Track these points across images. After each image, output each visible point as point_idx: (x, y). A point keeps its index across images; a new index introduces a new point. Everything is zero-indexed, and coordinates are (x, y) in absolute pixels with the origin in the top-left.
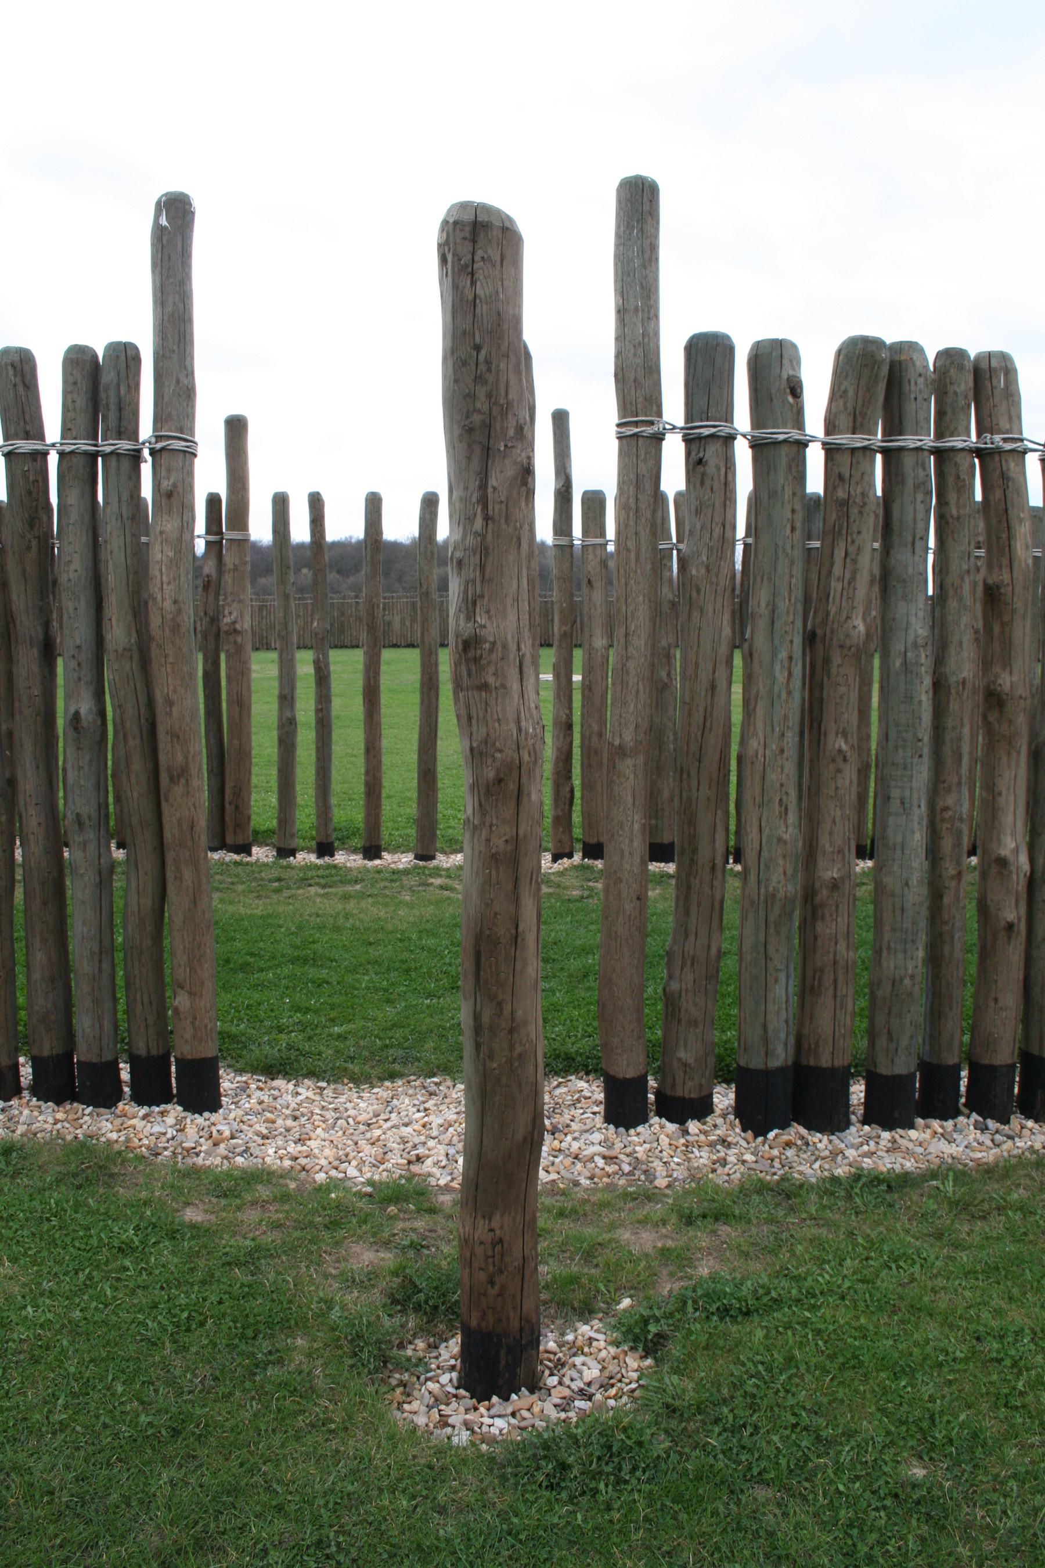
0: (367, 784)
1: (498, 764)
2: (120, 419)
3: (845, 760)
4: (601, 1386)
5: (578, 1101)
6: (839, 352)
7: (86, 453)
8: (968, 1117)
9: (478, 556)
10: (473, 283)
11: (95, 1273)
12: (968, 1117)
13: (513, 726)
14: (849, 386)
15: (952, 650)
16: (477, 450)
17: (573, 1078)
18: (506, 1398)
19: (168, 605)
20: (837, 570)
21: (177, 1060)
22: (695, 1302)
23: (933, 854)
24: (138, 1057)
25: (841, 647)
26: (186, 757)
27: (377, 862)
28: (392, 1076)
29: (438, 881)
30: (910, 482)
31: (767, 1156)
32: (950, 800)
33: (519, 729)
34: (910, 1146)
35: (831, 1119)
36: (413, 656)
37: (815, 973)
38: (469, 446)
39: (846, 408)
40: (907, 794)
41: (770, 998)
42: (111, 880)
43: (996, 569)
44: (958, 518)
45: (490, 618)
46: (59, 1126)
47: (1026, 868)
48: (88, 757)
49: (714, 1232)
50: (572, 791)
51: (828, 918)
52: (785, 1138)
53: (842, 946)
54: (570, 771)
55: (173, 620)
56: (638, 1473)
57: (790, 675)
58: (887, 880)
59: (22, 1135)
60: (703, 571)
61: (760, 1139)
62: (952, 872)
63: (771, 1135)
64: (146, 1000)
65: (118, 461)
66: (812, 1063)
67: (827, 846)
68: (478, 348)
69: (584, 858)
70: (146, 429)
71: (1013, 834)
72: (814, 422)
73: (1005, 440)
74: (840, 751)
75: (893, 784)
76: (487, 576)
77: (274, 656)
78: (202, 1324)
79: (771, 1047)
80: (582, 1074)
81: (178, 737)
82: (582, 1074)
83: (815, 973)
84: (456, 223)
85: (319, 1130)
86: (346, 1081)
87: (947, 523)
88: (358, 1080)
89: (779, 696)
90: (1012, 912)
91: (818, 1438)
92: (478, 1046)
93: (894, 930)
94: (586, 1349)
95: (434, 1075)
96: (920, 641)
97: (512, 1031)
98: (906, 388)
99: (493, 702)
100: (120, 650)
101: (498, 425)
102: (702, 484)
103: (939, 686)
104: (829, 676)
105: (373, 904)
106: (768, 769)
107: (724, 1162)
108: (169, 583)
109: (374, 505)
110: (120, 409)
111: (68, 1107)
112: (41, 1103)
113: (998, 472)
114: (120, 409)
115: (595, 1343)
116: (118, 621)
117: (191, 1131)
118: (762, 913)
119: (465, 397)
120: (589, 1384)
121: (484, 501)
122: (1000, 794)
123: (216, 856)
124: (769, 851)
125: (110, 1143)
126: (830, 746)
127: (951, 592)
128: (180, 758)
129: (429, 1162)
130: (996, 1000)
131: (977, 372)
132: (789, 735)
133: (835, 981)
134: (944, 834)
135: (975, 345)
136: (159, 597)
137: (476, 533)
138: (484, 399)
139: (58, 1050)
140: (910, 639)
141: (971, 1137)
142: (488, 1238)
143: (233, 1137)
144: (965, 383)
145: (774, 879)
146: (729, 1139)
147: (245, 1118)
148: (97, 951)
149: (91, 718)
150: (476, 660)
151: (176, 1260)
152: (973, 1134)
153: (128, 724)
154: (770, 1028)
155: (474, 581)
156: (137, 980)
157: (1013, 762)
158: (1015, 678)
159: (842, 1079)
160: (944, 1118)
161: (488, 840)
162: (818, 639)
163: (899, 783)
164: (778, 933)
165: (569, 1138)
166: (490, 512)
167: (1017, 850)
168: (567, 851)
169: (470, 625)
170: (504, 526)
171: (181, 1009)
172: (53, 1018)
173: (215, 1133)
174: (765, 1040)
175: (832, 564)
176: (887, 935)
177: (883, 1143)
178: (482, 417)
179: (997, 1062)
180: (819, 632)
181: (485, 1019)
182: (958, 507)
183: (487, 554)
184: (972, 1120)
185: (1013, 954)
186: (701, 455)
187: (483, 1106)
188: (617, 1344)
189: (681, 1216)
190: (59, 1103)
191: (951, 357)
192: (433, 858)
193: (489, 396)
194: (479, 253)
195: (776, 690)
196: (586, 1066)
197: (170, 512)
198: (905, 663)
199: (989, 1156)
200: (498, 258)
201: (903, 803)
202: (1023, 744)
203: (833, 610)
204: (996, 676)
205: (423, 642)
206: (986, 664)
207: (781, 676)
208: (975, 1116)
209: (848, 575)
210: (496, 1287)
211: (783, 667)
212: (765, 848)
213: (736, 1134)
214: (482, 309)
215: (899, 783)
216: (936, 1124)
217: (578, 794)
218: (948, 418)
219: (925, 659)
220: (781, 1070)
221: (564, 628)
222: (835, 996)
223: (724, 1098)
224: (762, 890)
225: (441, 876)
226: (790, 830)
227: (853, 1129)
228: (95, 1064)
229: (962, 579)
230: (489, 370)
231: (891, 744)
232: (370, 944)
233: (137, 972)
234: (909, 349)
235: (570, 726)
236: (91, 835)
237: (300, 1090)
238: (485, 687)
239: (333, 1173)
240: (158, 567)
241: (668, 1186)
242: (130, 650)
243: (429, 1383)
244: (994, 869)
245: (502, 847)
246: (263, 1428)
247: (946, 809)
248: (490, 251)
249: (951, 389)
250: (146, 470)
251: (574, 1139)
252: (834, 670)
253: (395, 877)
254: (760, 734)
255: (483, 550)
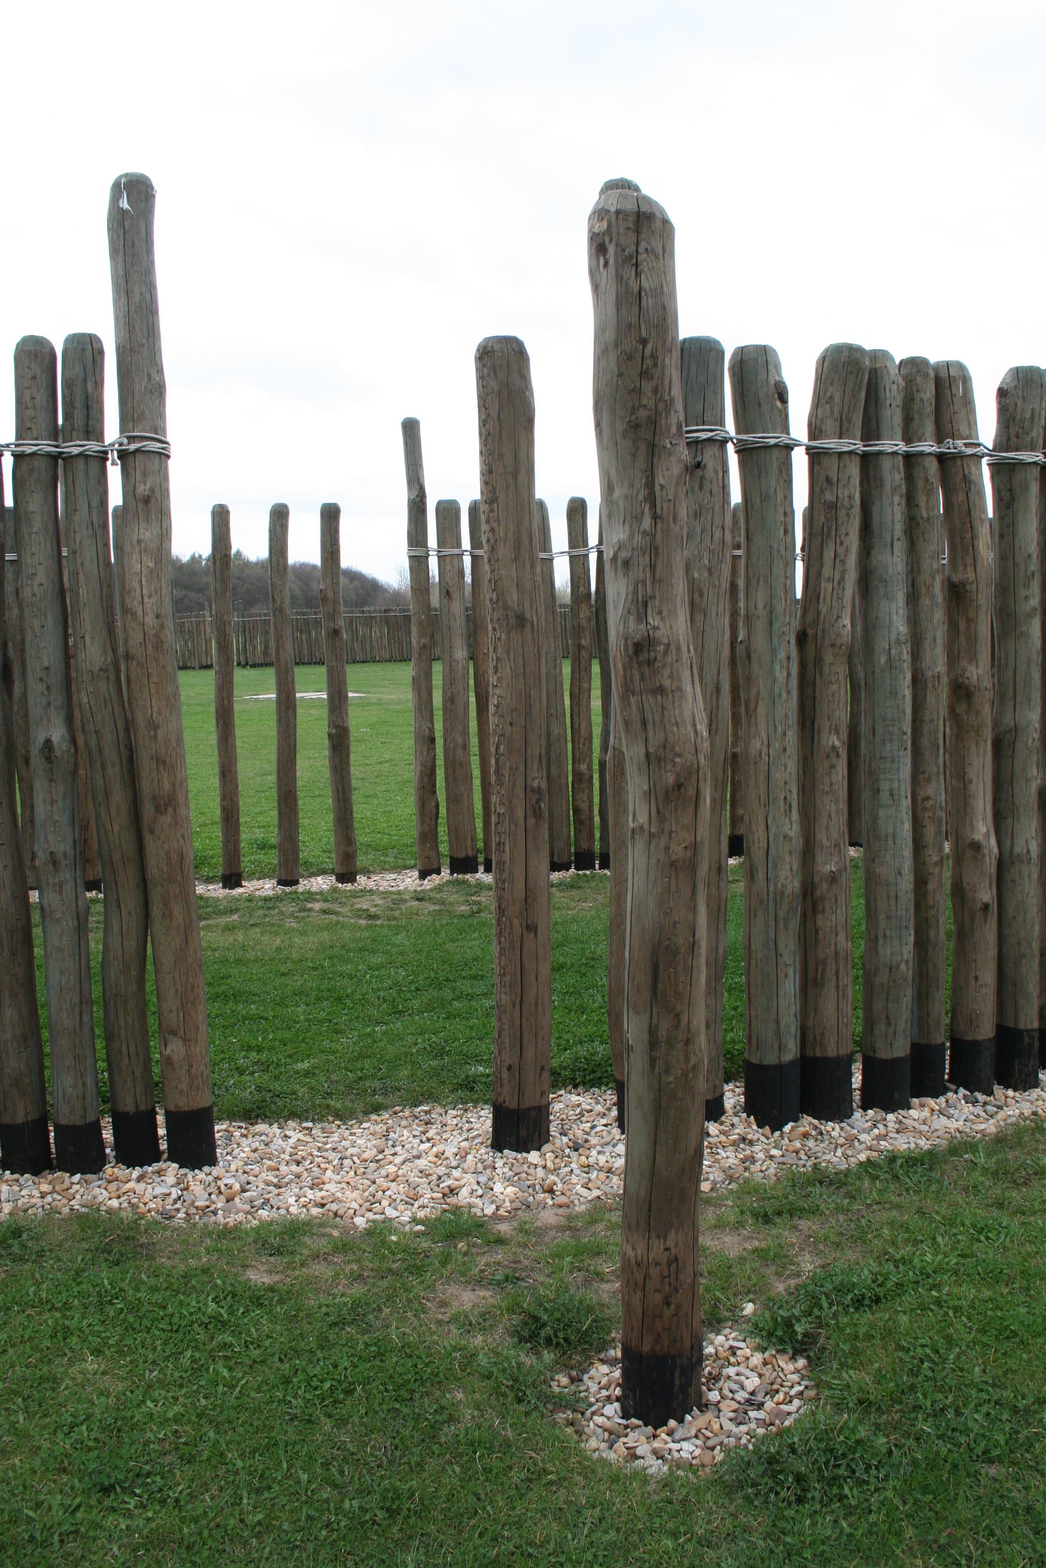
0: (224, 809)
1: (678, 768)
2: (88, 417)
3: (838, 756)
4: (767, 1394)
5: (582, 1114)
6: (823, 359)
7: (49, 455)
8: (956, 1093)
9: (647, 556)
10: (638, 275)
11: (197, 1355)
12: (956, 1093)
13: (690, 729)
14: (835, 391)
15: (927, 645)
16: (643, 446)
17: (562, 1092)
18: (681, 1421)
19: (150, 619)
20: (827, 571)
21: (168, 1114)
22: (827, 1296)
23: (919, 846)
24: (126, 1114)
25: (833, 646)
26: (174, 784)
27: (240, 890)
28: (377, 1109)
29: (317, 906)
30: (888, 486)
31: (791, 1149)
32: (930, 791)
33: (696, 732)
34: (916, 1124)
35: (836, 1109)
36: (269, 675)
37: (817, 965)
38: (634, 442)
39: (832, 413)
40: (896, 785)
41: (781, 992)
42: (87, 921)
43: (961, 568)
44: (928, 519)
45: (662, 619)
46: (49, 1199)
47: (996, 850)
48: (62, 789)
49: (795, 1228)
50: (437, 806)
51: (828, 911)
52: (801, 1129)
53: (841, 937)
54: (434, 786)
55: (156, 635)
56: (873, 1472)
57: (789, 674)
58: (882, 871)
59: (11, 1214)
60: (705, 574)
61: (777, 1133)
62: (935, 858)
63: (787, 1128)
64: (132, 1050)
65: (86, 464)
66: (818, 1054)
67: (824, 841)
68: (644, 342)
69: (452, 874)
70: (112, 431)
71: (984, 819)
72: (799, 428)
73: (966, 445)
74: (834, 747)
75: (882, 777)
76: (657, 577)
77: (322, 670)
78: (349, 1392)
79: (783, 1041)
80: (570, 1087)
81: (164, 763)
82: (570, 1087)
83: (817, 965)
84: (618, 212)
85: (329, 1173)
86: (331, 1119)
87: (918, 524)
88: (343, 1116)
89: (780, 696)
90: (986, 894)
91: (1015, 1411)
92: (653, 1061)
93: (889, 918)
94: (732, 1360)
95: (421, 1104)
96: (903, 639)
97: (688, 1042)
98: (882, 395)
99: (670, 706)
100: (96, 672)
101: (663, 422)
102: (701, 487)
103: (917, 681)
104: (821, 675)
105: (263, 934)
106: (772, 768)
107: (752, 1160)
108: (150, 596)
109: (221, 517)
110: (88, 407)
111: (50, 1177)
112: (17, 1176)
113: (961, 476)
114: (88, 407)
115: (739, 1352)
116: (93, 638)
117: (197, 1188)
118: (771, 909)
119: (630, 392)
120: (752, 1393)
121: (651, 499)
122: (971, 782)
123: (88, 895)
124: (777, 850)
125: (110, 1211)
126: (824, 742)
127: (924, 591)
128: (167, 786)
129: (464, 1192)
130: (976, 978)
131: (938, 381)
132: (790, 733)
133: (837, 971)
134: (926, 822)
135: (935, 356)
136: (140, 612)
137: (645, 532)
138: (650, 394)
139: (33, 1116)
140: (893, 636)
141: (966, 1110)
142: (664, 1258)
143: (244, 1191)
144: (928, 393)
145: (782, 879)
146: (749, 1137)
147: (248, 1168)
148: (77, 1002)
149: (64, 746)
150: (650, 663)
151: (278, 1328)
152: (968, 1109)
153: (107, 751)
154: (783, 1023)
155: (644, 582)
156: (123, 1031)
157: (981, 751)
158: (980, 672)
159: (843, 1065)
160: (935, 1095)
161: (667, 848)
162: (809, 639)
163: (888, 776)
164: (787, 929)
165: (594, 1153)
166: (658, 511)
167: (987, 835)
168: (435, 867)
169: (642, 626)
170: (672, 526)
171: (175, 1057)
172: (27, 1080)
173: (223, 1188)
174: (778, 1034)
175: (822, 566)
176: (883, 923)
177: (891, 1125)
178: (648, 413)
179: (980, 1038)
180: (810, 632)
181: (662, 1033)
182: (927, 509)
183: (657, 554)
184: (960, 1095)
185: (988, 933)
186: (699, 459)
187: (657, 1123)
188: (764, 1350)
189: (755, 1215)
190: (36, 1173)
191: (915, 366)
192: (296, 883)
193: (655, 391)
194: (643, 245)
195: (777, 690)
196: (574, 1079)
197: (148, 519)
198: (889, 660)
199: (990, 1127)
200: (660, 251)
201: (892, 795)
202: (988, 734)
203: (824, 609)
204: (964, 670)
205: (278, 659)
206: (952, 659)
207: (780, 676)
208: (962, 1091)
209: (837, 576)
210: (672, 1307)
211: (782, 667)
212: (772, 846)
213: (754, 1132)
214: (648, 302)
215: (888, 776)
216: (931, 1101)
217: (443, 811)
218: (914, 424)
219: (905, 654)
220: (792, 1063)
221: (423, 640)
222: (838, 987)
223: (733, 1096)
224: (772, 888)
225: (318, 901)
226: (793, 829)
227: (858, 1114)
228: (78, 1127)
229: (934, 578)
230: (655, 365)
231: (878, 739)
232: (283, 974)
233: (122, 1022)
234: (880, 356)
235: (433, 740)
236: (66, 875)
237: (288, 1133)
238: (661, 690)
239: (370, 1215)
240: (137, 579)
241: (712, 1189)
242: (106, 670)
243: (595, 1418)
244: (969, 854)
245: (681, 854)
246: (480, 1491)
247: (928, 798)
248: (653, 242)
249: (918, 397)
250: (114, 474)
251: (599, 1153)
252: (826, 669)
253: (270, 905)
254: (763, 734)
255: (654, 550)
